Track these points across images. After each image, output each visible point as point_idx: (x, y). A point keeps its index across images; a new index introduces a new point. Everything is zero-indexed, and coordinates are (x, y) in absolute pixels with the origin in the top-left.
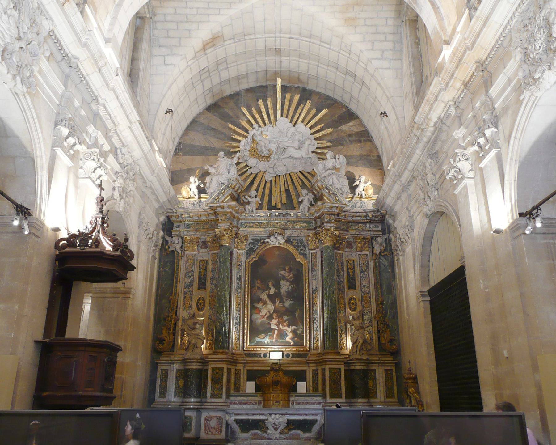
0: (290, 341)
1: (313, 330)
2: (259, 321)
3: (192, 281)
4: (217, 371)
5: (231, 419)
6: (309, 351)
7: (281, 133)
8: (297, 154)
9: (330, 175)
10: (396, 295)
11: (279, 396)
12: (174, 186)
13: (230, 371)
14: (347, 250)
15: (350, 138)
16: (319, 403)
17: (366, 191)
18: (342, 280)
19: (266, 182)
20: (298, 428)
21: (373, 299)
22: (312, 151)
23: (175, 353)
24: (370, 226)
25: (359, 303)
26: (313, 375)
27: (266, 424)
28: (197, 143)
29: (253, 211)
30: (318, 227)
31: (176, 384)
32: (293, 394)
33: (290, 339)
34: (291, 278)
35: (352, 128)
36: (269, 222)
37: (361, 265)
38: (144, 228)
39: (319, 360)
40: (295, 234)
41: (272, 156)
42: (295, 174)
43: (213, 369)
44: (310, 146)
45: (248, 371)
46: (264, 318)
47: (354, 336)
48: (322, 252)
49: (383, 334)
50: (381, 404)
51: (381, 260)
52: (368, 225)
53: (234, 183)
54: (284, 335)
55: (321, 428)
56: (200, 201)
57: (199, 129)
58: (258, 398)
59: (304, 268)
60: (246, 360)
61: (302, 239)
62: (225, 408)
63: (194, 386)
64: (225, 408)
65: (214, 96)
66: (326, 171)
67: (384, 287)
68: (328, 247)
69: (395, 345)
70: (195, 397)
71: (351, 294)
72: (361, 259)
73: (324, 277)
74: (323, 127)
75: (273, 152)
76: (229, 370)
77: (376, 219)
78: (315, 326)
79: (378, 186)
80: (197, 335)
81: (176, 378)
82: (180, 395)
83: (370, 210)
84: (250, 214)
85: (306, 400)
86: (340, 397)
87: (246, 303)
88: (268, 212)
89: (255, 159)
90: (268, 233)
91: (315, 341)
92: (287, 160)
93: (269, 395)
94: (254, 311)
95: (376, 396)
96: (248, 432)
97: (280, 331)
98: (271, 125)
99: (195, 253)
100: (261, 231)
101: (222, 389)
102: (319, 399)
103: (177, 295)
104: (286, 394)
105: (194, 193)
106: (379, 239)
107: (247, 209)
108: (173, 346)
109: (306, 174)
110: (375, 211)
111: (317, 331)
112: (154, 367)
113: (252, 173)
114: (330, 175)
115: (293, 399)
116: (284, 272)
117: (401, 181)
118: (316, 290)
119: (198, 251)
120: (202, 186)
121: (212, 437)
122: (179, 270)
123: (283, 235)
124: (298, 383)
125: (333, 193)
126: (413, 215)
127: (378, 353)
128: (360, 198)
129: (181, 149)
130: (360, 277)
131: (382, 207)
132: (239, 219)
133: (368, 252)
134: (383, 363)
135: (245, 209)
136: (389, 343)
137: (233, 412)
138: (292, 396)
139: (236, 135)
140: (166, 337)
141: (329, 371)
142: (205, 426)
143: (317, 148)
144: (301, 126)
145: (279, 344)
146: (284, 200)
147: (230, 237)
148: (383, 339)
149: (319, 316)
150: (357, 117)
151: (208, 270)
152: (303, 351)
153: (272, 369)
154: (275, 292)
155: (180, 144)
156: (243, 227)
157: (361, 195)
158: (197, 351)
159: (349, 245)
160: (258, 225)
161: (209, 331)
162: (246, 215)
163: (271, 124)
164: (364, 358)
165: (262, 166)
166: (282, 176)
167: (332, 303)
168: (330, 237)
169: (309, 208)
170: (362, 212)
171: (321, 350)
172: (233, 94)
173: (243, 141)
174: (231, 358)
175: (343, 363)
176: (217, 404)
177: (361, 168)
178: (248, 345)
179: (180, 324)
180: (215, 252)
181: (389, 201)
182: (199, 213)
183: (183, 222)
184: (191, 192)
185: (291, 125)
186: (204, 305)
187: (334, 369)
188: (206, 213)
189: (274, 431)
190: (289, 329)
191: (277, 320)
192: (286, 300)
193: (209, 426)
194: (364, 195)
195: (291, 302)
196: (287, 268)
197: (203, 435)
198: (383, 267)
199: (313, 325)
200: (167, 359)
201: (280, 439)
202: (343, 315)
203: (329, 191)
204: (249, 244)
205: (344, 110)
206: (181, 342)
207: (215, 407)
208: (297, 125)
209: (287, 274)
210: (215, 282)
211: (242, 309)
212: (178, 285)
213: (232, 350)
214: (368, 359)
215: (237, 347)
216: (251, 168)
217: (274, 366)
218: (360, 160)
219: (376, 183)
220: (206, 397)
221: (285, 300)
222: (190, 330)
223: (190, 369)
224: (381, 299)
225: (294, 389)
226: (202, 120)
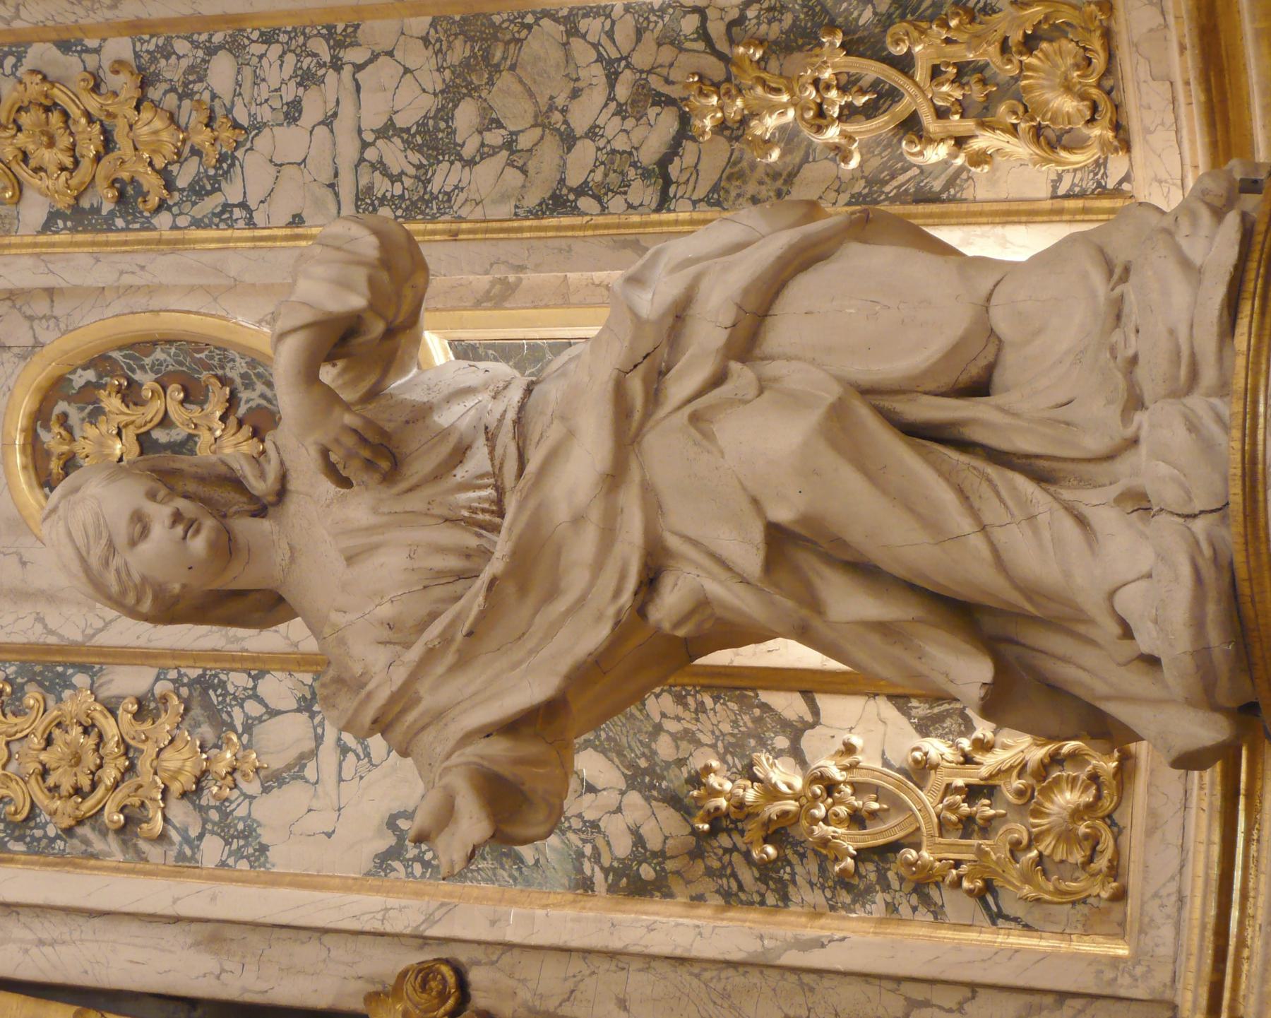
80: (657, 378)
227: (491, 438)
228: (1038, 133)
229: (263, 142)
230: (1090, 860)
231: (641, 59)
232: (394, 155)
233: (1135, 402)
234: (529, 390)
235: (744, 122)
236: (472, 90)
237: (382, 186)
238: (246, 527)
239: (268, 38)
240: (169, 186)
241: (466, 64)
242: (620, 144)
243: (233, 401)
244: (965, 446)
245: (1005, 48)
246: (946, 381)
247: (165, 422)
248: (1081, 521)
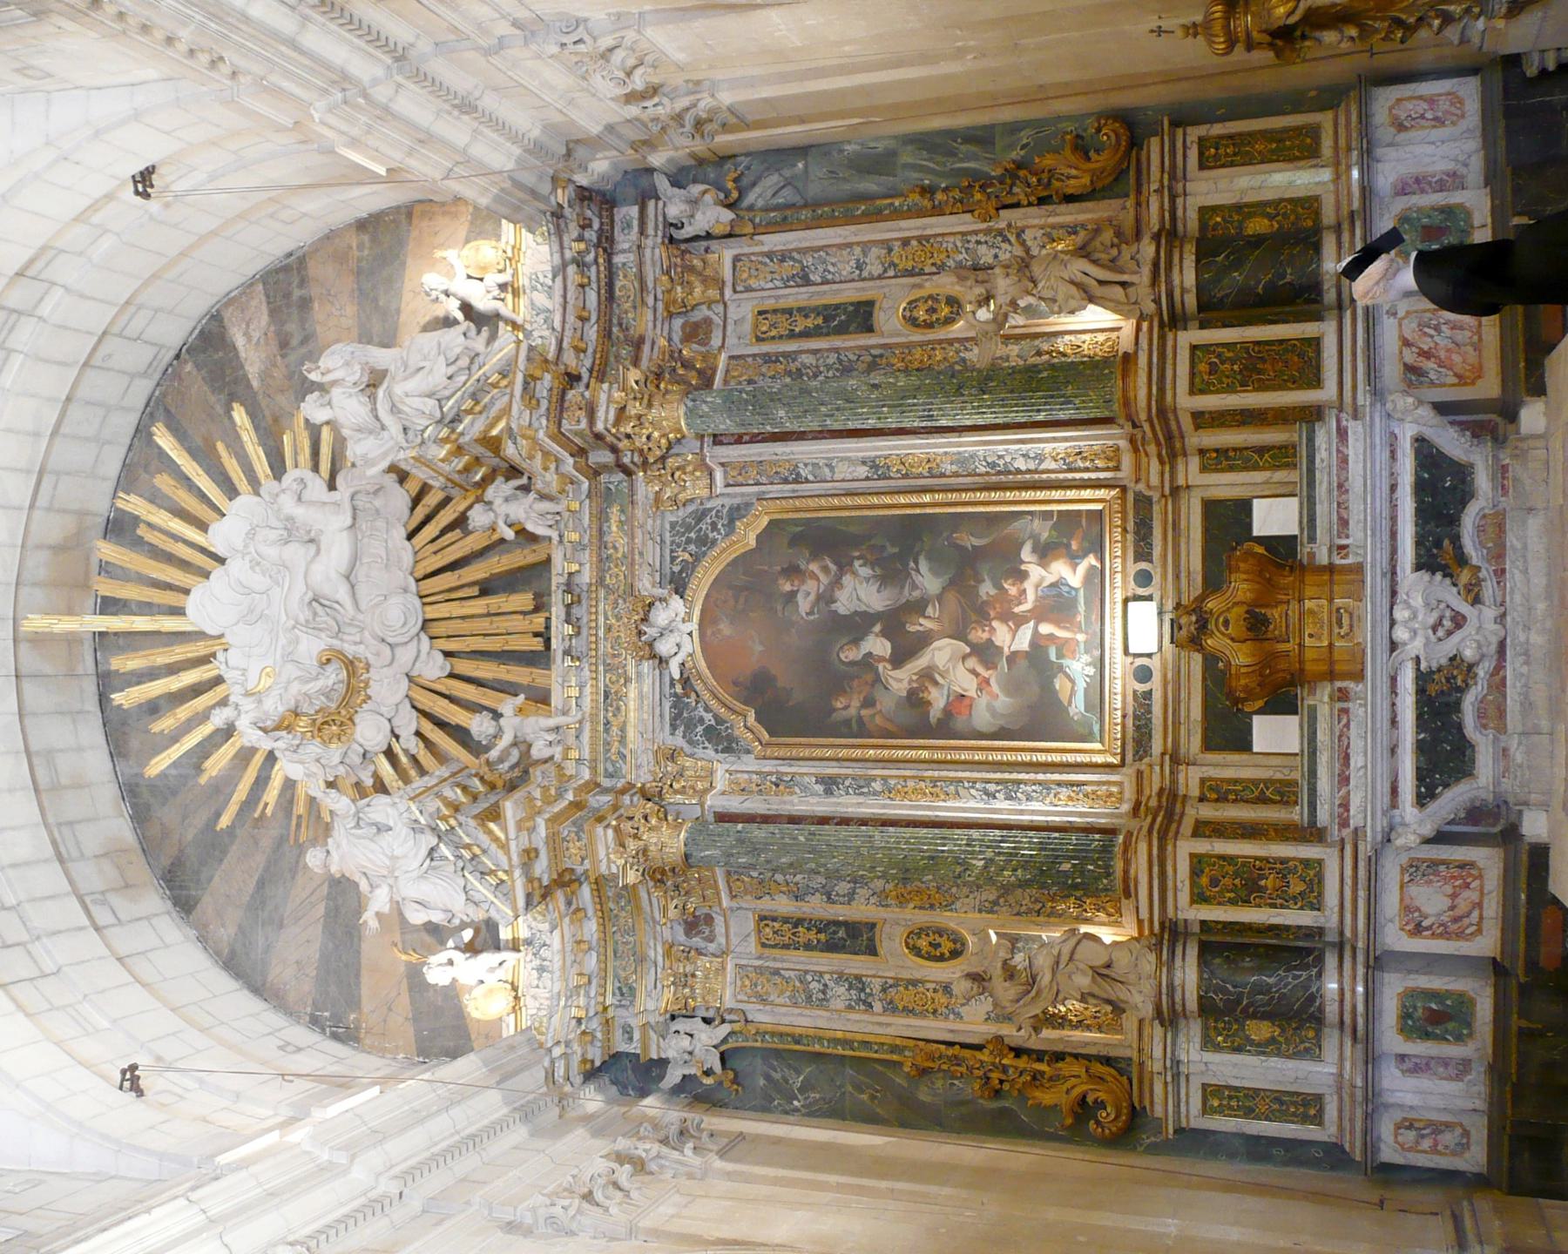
0: (1082, 567)
1: (1036, 471)
2: (1003, 702)
3: (841, 977)
4: (1204, 880)
5: (1415, 821)
6: (1124, 489)
7: (251, 617)
8: (337, 549)
9: (394, 409)
10: (895, 137)
11: (1311, 612)
12: (475, 1045)
13: (1207, 823)
14: (716, 341)
15: (294, 342)
16: (1342, 433)
17: (484, 269)
18: (832, 359)
19: (452, 676)
20: (1453, 521)
21: (911, 227)
22: (325, 487)
23: (1135, 1055)
24: (624, 251)
25: (932, 286)
26: (1223, 471)
27: (1434, 666)
28: (313, 952)
29: (557, 729)
30: (618, 459)
31: (1263, 1053)
32: (1303, 551)
33: (1074, 567)
34: (825, 569)
35: (256, 335)
36: (606, 665)
37: (778, 283)
38: (572, 1212)
39: (1158, 444)
40: (652, 554)
41: (350, 650)
42: (420, 556)
43: (1199, 898)
44: (306, 496)
45: (1208, 746)
46: (987, 681)
47: (1060, 297)
48: (717, 440)
49: (1056, 184)
50: (1344, 178)
51: (760, 203)
52: (618, 259)
53: (434, 804)
54: (1060, 595)
55: (1452, 423)
56: (529, 942)
57: (261, 942)
58: (1321, 699)
59: (785, 516)
60: (1163, 754)
61: (673, 525)
62: (1365, 849)
63: (1271, 980)
64: (1365, 849)
65: (127, 886)
66: (383, 428)
67: (869, 185)
68: (690, 414)
69: (1099, 130)
70: (1320, 975)
71: (890, 322)
72: (753, 283)
73: (815, 426)
74: (228, 447)
75: (331, 649)
76: (1203, 829)
77: (596, 226)
78: (1021, 464)
79: (472, 223)
80: (1058, 963)
81: (1238, 1050)
82: (1311, 1034)
83: (556, 247)
84: (571, 740)
85: (1330, 491)
86: (1315, 343)
87: (925, 754)
88: (560, 664)
89: (357, 719)
90: (646, 666)
91: (1080, 464)
92: (362, 590)
93: (1309, 655)
94: (959, 723)
95: (1310, 204)
96: (1472, 747)
97: (1040, 614)
98: (220, 656)
99: (730, 967)
100: (641, 696)
101: (1283, 861)
102: (1324, 437)
103: (898, 1042)
104: (1302, 581)
105: (492, 970)
106: (674, 211)
107: (546, 753)
108: (1107, 1061)
109: (421, 512)
110: (558, 227)
111: (1040, 458)
112: (1192, 1141)
113: (418, 734)
114: (394, 409)
115: (1325, 550)
116: (800, 597)
117: (376, 82)
118: (873, 464)
119: (723, 953)
120: (468, 935)
121: (1492, 907)
122: (798, 1031)
123: (651, 605)
124: (1257, 531)
125: (475, 397)
126: (515, 24)
127: (1130, 203)
128: (516, 293)
129: (337, 1019)
130: (822, 284)
131: (534, 193)
132: (593, 786)
133: (725, 255)
134: (1173, 177)
135: (546, 761)
136: (1092, 154)
137: (1384, 813)
138: (1312, 555)
139: (265, 798)
140: (1068, 1092)
141: (1202, 392)
142: (1446, 935)
143: (316, 468)
144: (220, 536)
145: (1095, 617)
146: (523, 600)
147: (654, 821)
148: (1072, 182)
149: (981, 450)
150: (216, 318)
151: (799, 915)
152: (1124, 512)
153: (1195, 642)
154: (885, 634)
155: (315, 1022)
156: (625, 769)
157: (503, 287)
158: (1123, 961)
159: (697, 332)
160: (618, 709)
161: (1042, 912)
162: (574, 754)
163: (214, 655)
164: (1148, 249)
165: (387, 690)
166: (428, 608)
167: (916, 391)
168: (650, 405)
169: (543, 497)
170: (565, 279)
171: (1113, 437)
172: (133, 806)
173: (286, 768)
174: (1149, 819)
175: (1170, 336)
176: (1348, 881)
177: (407, 296)
178: (1098, 746)
179: (1014, 1034)
181: (501, 157)
182: (568, 949)
183: (611, 1013)
184: (492, 980)
185: (218, 572)
186: (940, 932)
187: (1192, 374)
188: (567, 920)
189: (1469, 629)
190: (1035, 572)
191: (995, 624)
192: (914, 586)
193: (1445, 918)
194: (505, 277)
195: (924, 566)
196: (787, 587)
197: (1487, 944)
198: (785, 192)
199: (1018, 471)
200: (1158, 1088)
201: (1502, 604)
202: (976, 350)
203: (469, 412)
204: (690, 742)
205: (189, 367)
206: (1088, 1028)
207: (1362, 894)
208: (220, 550)
209: (811, 586)
210: (843, 887)
211: (952, 774)
212: (859, 1037)
213: (1120, 816)
214: (1156, 237)
215: (1111, 795)
216: (397, 737)
217: (1184, 632)
218: (375, 300)
219: (462, 233)
220: (1321, 931)
221: (916, 594)
222: (1039, 993)
223: (1200, 998)
224: (915, 198)
225: (1281, 550)
226: (225, 933)
230: (711, 486)
232: (987, 904)
238: (986, 984)
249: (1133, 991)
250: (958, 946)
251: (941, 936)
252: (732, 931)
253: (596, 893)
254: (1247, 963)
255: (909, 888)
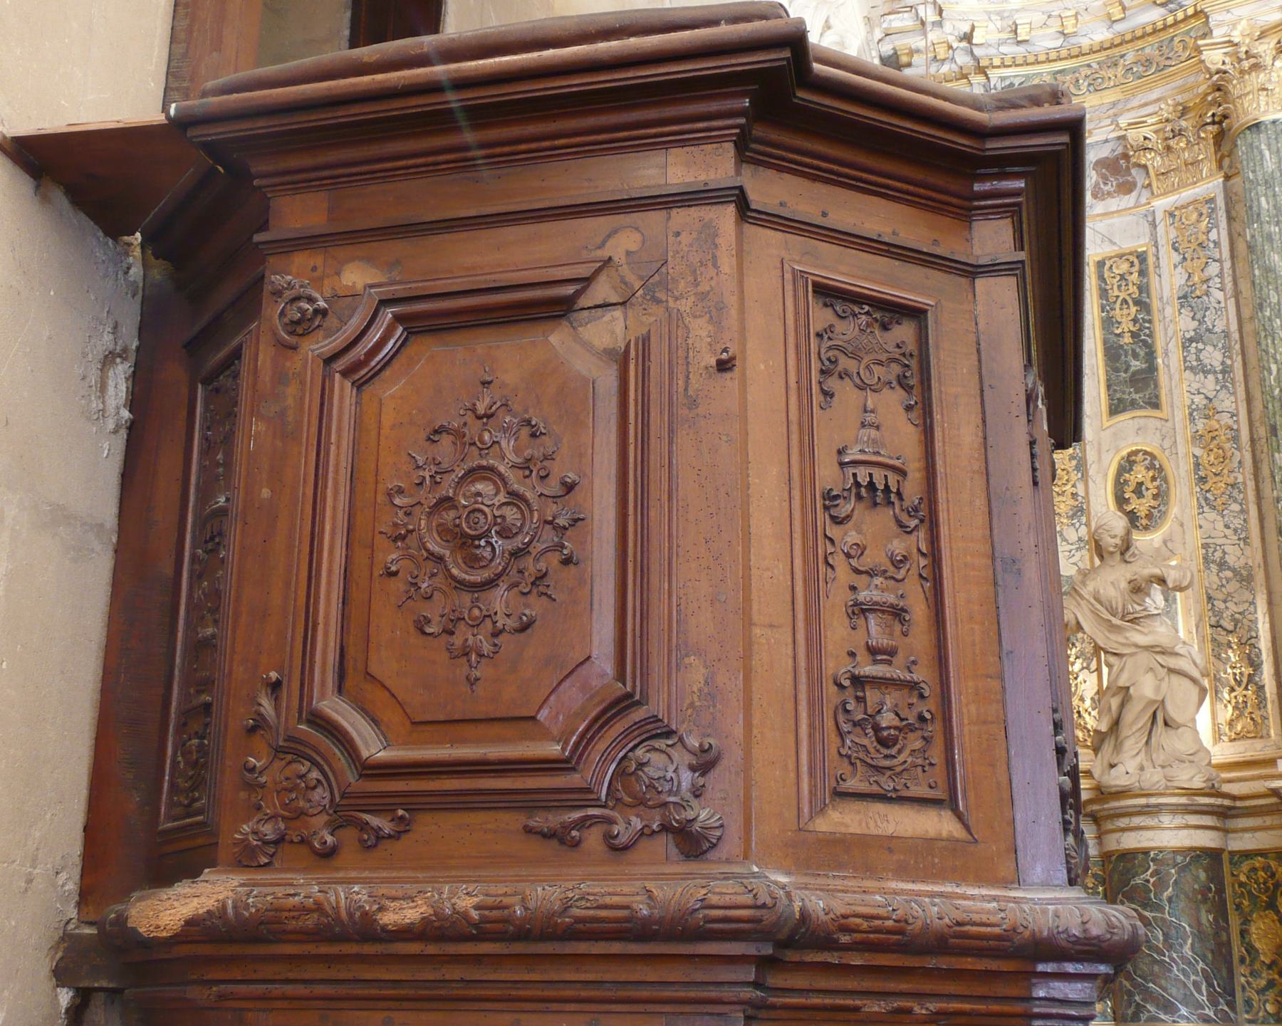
63: (1187, 950)
151: (1156, 304)
180: (1187, 194)
223: (1146, 852)
227: (1144, 610)
228: (1232, 720)
229: (1219, 518)
231: (1245, 620)
232: (1218, 554)
233: (1163, 767)
234: (1159, 614)
235: (1231, 648)
236: (1235, 575)
237: (1211, 550)
238: (1118, 556)
239: (1245, 520)
240: (1207, 491)
241: (1241, 575)
242: (1225, 615)
243: (1154, 508)
244: (1153, 723)
245: (1251, 713)
246: (1167, 718)
247: (1147, 489)
248: (1138, 754)
249: (1138, 759)
250: (1144, 522)
251: (1155, 497)
252: (1115, 220)
253: (1149, 29)
254: (1207, 918)
255: (1227, 446)
